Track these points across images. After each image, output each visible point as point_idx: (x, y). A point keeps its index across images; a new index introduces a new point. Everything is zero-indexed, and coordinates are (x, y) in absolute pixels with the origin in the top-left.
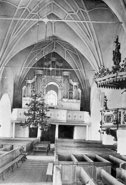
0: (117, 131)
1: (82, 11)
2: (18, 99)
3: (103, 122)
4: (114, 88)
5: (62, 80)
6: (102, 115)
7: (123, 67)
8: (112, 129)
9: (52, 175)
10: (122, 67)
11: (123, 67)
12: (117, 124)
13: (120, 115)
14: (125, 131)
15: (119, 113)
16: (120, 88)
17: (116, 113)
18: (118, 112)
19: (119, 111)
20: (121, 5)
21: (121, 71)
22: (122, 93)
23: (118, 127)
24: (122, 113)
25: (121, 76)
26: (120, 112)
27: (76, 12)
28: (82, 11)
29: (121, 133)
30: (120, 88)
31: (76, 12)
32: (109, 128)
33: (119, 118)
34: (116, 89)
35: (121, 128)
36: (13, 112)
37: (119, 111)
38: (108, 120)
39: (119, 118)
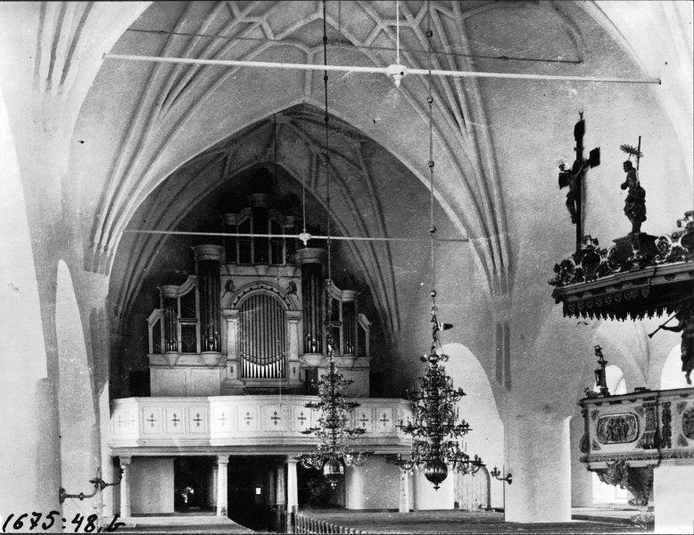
0: (656, 471)
1: (438, 11)
2: (48, 306)
3: (591, 442)
4: (612, 317)
5: (295, 280)
6: (585, 416)
7: (679, 244)
8: (635, 464)
9: (172, 460)
10: (675, 245)
11: (679, 244)
12: (656, 446)
13: (667, 417)
14: (692, 468)
15: (661, 409)
16: (629, 317)
17: (652, 409)
18: (657, 404)
19: (664, 399)
20: (294, 99)
21: (670, 260)
22: (651, 336)
23: (661, 457)
24: (673, 408)
25: (667, 276)
26: (667, 405)
27: (415, 16)
28: (438, 11)
29: (672, 480)
30: (629, 317)
31: (415, 16)
32: (623, 463)
33: (661, 425)
34: (618, 318)
35: (673, 460)
36: (117, 413)
37: (664, 399)
38: (615, 432)
39: (661, 425)
